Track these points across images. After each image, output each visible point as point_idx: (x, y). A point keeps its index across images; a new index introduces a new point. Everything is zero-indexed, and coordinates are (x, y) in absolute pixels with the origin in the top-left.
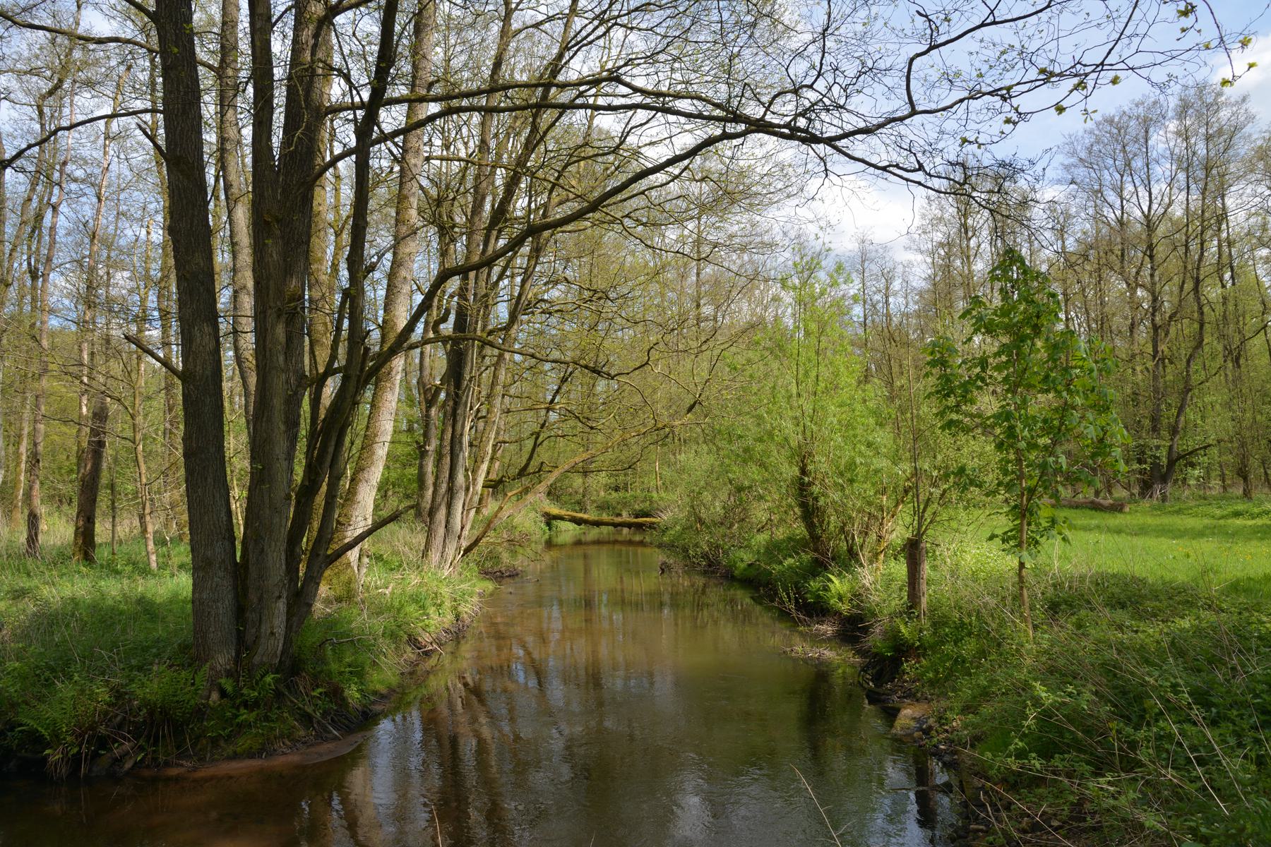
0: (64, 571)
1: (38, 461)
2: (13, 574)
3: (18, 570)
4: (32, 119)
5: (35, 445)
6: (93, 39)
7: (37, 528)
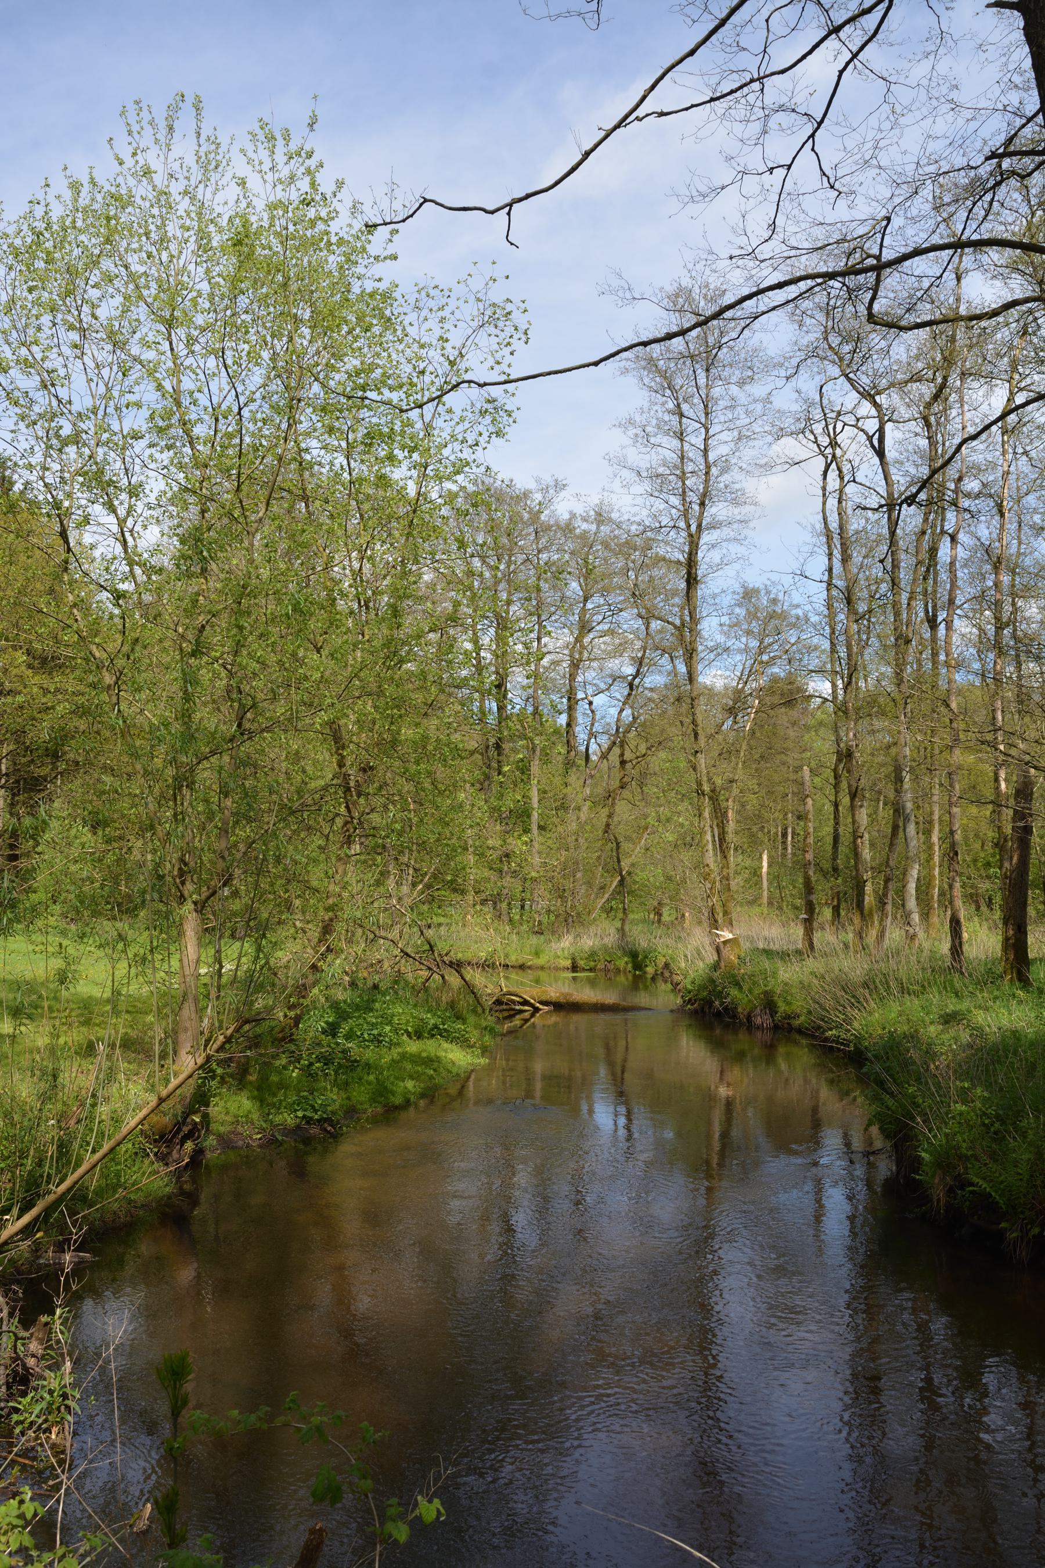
0: (996, 993)
1: (956, 854)
2: (940, 993)
3: (945, 988)
4: (917, 434)
5: (952, 833)
6: (986, 314)
7: (960, 937)
